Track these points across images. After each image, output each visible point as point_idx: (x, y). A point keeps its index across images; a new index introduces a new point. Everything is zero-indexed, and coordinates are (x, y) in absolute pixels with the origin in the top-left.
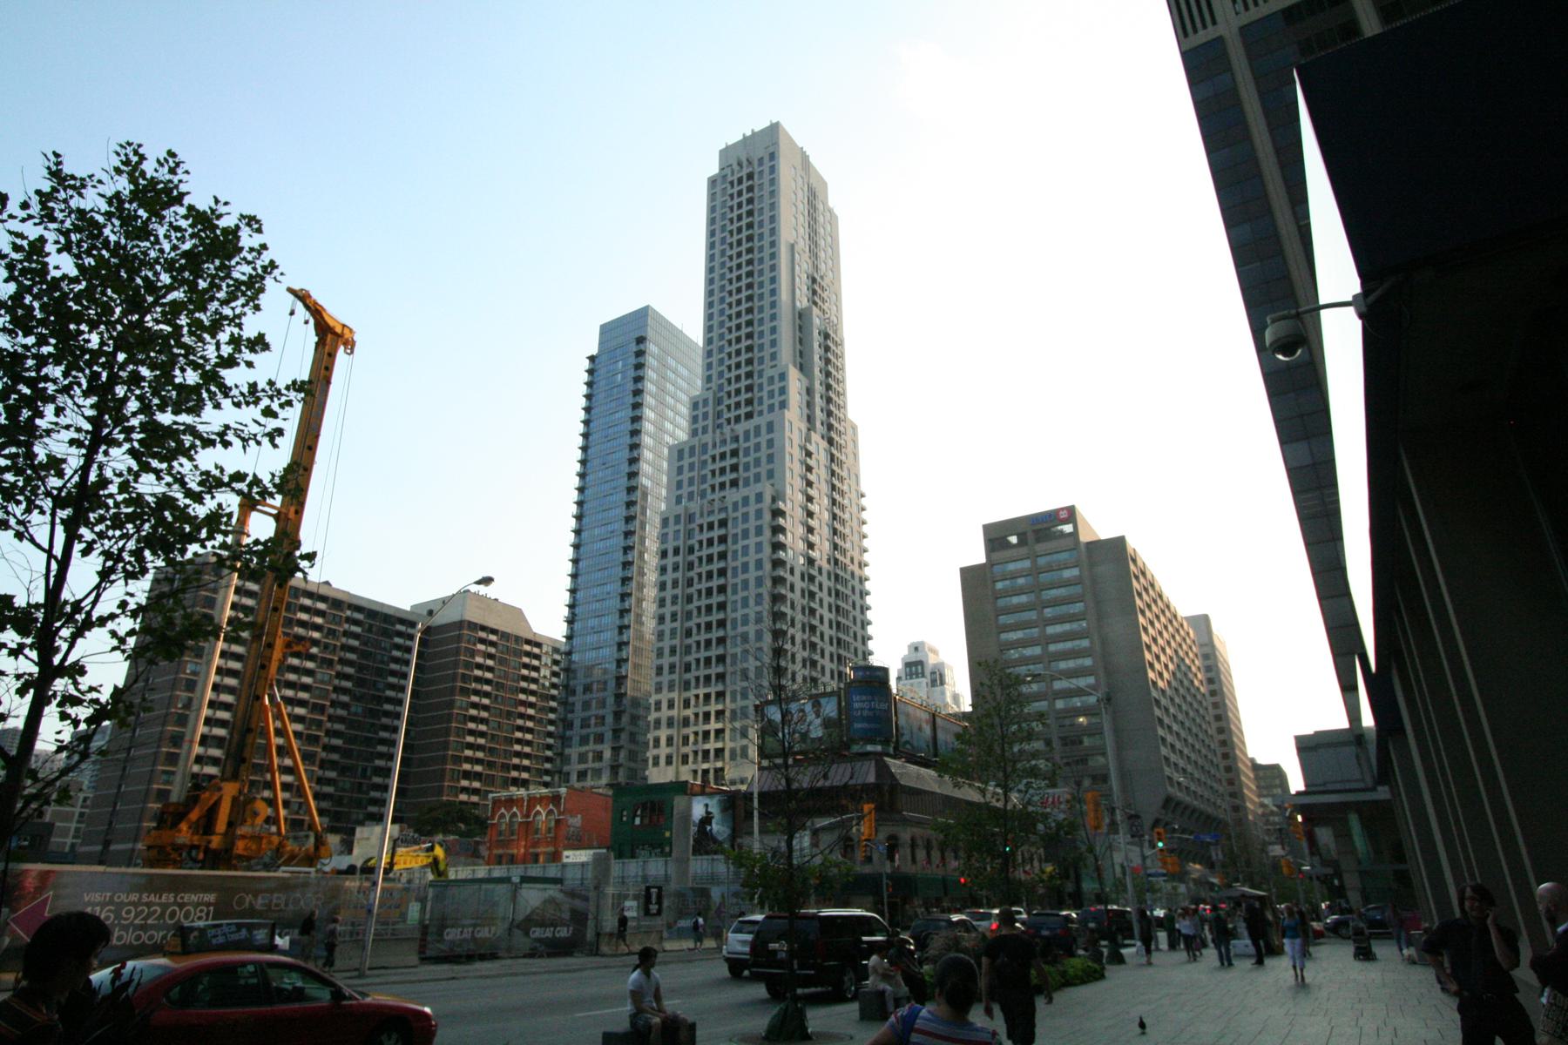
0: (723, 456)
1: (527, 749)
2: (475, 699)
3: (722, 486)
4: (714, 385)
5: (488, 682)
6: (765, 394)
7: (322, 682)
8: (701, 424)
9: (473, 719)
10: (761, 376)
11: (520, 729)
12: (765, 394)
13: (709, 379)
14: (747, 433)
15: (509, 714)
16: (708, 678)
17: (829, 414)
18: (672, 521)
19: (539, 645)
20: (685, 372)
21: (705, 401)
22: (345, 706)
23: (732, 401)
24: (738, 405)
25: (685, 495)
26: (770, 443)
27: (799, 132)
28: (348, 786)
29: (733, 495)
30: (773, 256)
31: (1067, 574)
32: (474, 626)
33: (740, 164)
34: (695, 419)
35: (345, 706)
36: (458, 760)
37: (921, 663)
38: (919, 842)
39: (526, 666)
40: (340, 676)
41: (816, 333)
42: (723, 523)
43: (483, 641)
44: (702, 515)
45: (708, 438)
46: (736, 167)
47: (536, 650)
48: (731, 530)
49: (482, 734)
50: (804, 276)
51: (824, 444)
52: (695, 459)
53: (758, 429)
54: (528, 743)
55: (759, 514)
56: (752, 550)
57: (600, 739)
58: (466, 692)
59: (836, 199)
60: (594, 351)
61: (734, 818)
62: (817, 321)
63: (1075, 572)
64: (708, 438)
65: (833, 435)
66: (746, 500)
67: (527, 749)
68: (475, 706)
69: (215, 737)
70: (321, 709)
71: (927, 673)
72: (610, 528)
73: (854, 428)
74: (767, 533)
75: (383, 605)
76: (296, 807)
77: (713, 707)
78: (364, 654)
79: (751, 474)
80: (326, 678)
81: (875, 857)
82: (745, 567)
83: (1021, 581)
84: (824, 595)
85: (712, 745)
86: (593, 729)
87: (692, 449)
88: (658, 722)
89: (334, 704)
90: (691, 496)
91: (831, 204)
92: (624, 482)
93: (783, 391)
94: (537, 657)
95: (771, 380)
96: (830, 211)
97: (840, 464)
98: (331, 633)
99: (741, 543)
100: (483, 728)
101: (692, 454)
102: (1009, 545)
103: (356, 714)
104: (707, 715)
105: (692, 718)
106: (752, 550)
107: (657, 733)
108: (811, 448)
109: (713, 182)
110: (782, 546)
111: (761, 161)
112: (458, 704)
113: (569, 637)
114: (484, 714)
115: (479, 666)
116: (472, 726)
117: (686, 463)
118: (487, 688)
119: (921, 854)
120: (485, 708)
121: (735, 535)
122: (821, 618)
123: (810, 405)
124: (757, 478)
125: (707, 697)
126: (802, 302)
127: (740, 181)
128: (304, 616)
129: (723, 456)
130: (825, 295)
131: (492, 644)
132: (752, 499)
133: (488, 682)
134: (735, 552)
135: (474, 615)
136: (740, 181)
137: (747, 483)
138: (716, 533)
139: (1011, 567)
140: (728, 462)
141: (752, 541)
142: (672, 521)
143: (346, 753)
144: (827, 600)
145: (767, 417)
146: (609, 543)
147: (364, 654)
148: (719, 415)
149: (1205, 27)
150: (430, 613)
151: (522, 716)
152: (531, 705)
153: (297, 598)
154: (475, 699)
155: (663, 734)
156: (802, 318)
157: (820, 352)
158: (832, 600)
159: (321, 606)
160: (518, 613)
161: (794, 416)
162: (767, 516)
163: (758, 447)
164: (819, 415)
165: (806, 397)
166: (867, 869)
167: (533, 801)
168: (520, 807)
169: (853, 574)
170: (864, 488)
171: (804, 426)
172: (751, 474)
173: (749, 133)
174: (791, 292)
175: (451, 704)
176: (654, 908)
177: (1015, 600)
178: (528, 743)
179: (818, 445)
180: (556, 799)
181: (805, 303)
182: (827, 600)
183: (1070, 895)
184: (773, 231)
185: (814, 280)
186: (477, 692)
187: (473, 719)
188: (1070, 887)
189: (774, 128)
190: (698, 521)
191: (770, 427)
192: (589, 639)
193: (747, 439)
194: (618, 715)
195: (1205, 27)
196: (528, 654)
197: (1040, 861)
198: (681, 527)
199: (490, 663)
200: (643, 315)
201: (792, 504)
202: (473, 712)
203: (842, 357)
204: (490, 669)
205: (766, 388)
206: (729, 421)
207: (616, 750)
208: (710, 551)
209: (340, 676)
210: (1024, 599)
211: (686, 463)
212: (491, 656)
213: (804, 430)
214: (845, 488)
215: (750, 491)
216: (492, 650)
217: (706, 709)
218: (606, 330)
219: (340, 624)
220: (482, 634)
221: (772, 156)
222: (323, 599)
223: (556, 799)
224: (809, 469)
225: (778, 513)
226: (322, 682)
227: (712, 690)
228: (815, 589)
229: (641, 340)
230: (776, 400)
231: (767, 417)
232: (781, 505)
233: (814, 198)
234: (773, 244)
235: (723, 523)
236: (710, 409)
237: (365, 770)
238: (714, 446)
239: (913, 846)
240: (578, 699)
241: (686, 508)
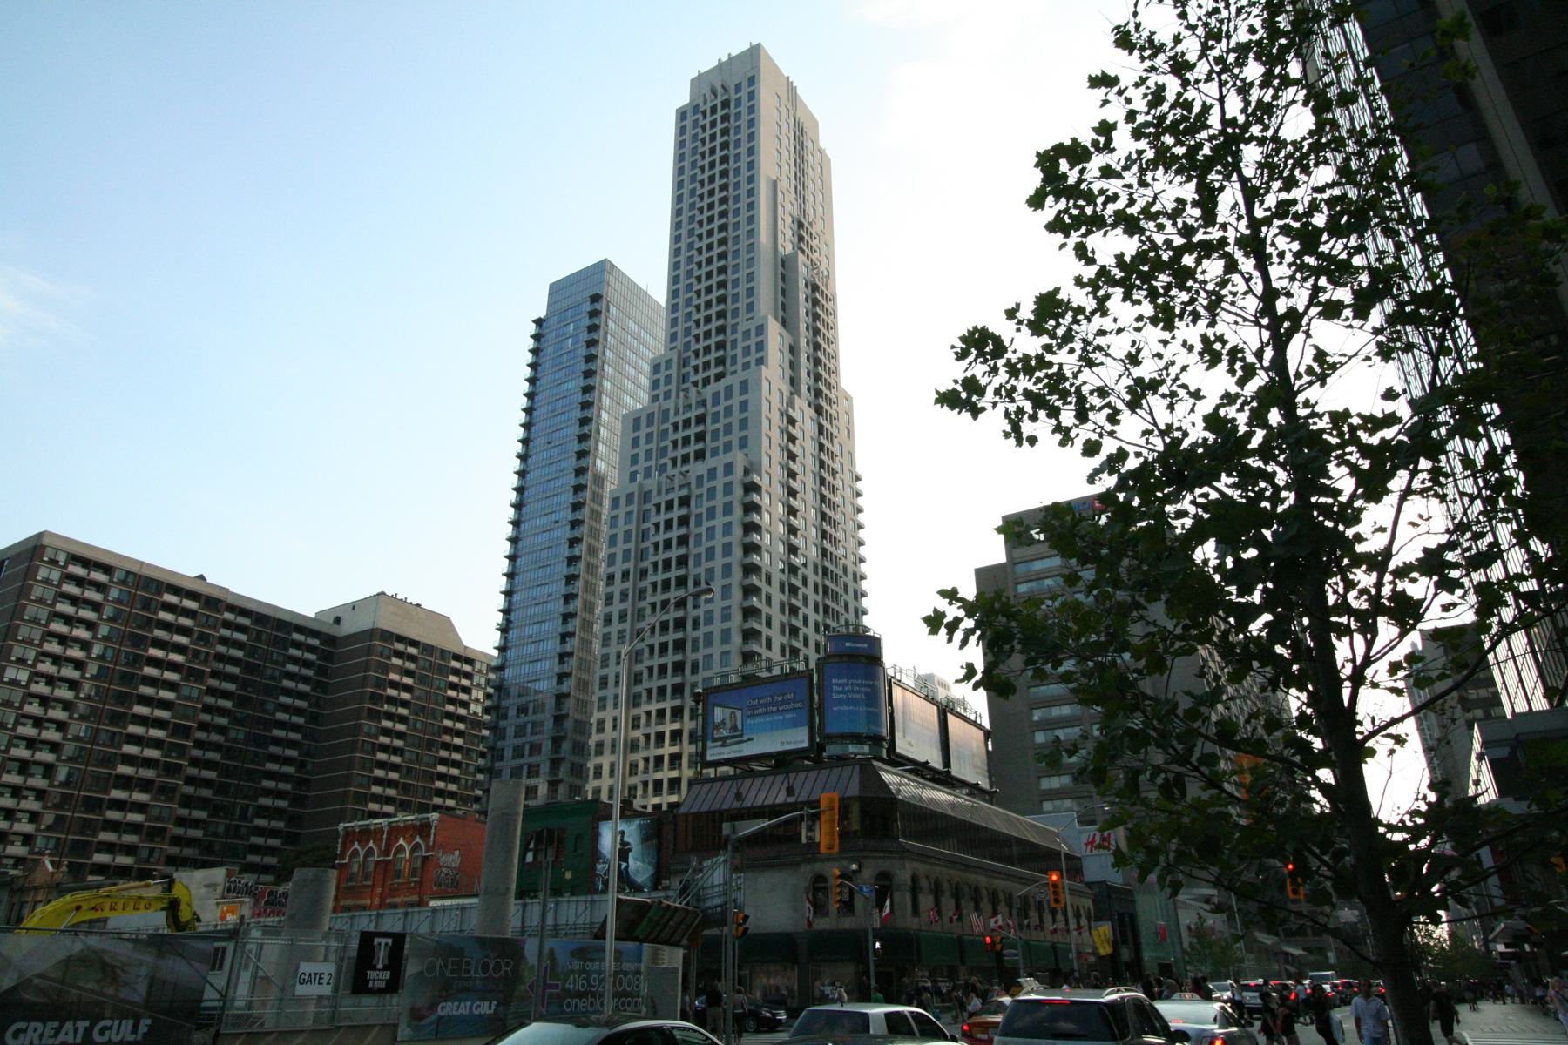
0: (687, 423)
1: (452, 787)
2: (387, 724)
3: (685, 459)
4: (679, 344)
5: (404, 704)
6: (739, 351)
7: (189, 698)
8: (663, 388)
9: (385, 748)
10: (734, 331)
11: (444, 762)
12: (739, 351)
13: (673, 337)
14: (716, 395)
15: (430, 744)
16: (662, 691)
17: (818, 378)
18: (623, 501)
19: (470, 661)
20: (649, 340)
21: (668, 363)
22: (222, 730)
23: (700, 362)
24: (707, 366)
25: (641, 471)
26: (744, 406)
27: (785, 58)
28: (221, 829)
29: (698, 468)
30: (751, 193)
32: (387, 636)
33: (714, 92)
34: (655, 384)
35: (222, 730)
36: (364, 798)
38: (924, 883)
39: (453, 686)
40: (212, 691)
41: (802, 283)
42: (684, 501)
43: (399, 654)
44: (659, 493)
45: (670, 405)
46: (709, 96)
47: (467, 668)
48: (694, 509)
49: (395, 767)
50: (789, 220)
51: (810, 412)
52: (654, 429)
53: (729, 389)
54: (454, 779)
55: (728, 488)
56: (719, 531)
57: (533, 771)
58: (375, 715)
59: (828, 139)
60: (542, 314)
61: (659, 849)
62: (802, 270)
64: (670, 405)
65: (822, 402)
66: (712, 473)
67: (452, 787)
68: (387, 732)
69: (199, 798)
70: (184, 731)
72: (555, 517)
73: (848, 399)
74: (738, 512)
75: (276, 608)
76: (145, 854)
77: (669, 727)
78: (249, 668)
79: (720, 444)
80: (195, 694)
81: (859, 903)
82: (710, 553)
84: (810, 591)
85: (666, 774)
86: (527, 760)
87: (650, 416)
88: (600, 746)
89: (203, 726)
90: (648, 473)
91: (823, 144)
92: (572, 462)
93: (761, 346)
94: (468, 676)
95: (747, 334)
96: (821, 152)
97: (831, 438)
98: (203, 638)
99: (706, 524)
100: (396, 759)
101: (650, 422)
102: (1032, 542)
103: (235, 741)
104: (660, 737)
105: (642, 739)
106: (719, 531)
107: (599, 760)
108: (796, 415)
109: (682, 114)
110: (756, 528)
111: (738, 88)
112: (366, 729)
113: (502, 649)
114: (399, 743)
115: (394, 685)
116: (382, 756)
117: (643, 433)
118: (403, 711)
119: (926, 901)
120: (400, 735)
121: (699, 516)
122: (806, 618)
123: (793, 366)
124: (728, 447)
125: (661, 713)
126: (786, 248)
127: (714, 110)
128: (167, 616)
129: (687, 423)
130: (814, 243)
131: (412, 658)
132: (720, 471)
133: (404, 704)
134: (699, 536)
136: (714, 110)
137: (715, 452)
138: (676, 513)
139: (1037, 566)
140: (693, 430)
141: (719, 521)
142: (623, 501)
143: (221, 789)
144: (812, 597)
145: (741, 375)
146: (554, 534)
147: (249, 668)
148: (684, 378)
150: (338, 620)
151: (446, 746)
152: (459, 734)
153: (160, 594)
154: (387, 724)
155: (605, 761)
156: (785, 267)
157: (807, 307)
158: (819, 598)
159: (191, 604)
160: (444, 623)
161: (773, 374)
162: (738, 491)
163: (728, 411)
164: (805, 380)
165: (788, 356)
166: (847, 923)
167: (395, 832)
168: (378, 841)
169: (845, 569)
170: (860, 469)
171: (786, 388)
172: (720, 444)
173: (725, 58)
174: (771, 233)
175: (357, 729)
176: (378, 977)
178: (454, 779)
179: (803, 411)
180: (423, 829)
181: (789, 249)
182: (812, 597)
183: (1127, 964)
184: (751, 165)
185: (801, 225)
186: (390, 716)
187: (385, 748)
188: (1126, 954)
189: (755, 52)
190: (655, 500)
191: (744, 387)
192: (526, 650)
193: (716, 402)
194: (557, 741)
196: (456, 672)
197: (1089, 918)
198: (634, 508)
199: (408, 681)
200: (602, 269)
201: (771, 479)
202: (384, 740)
203: (834, 314)
204: (407, 688)
205: (740, 345)
206: (695, 384)
207: (553, 785)
208: (668, 535)
209: (212, 691)
211: (643, 433)
212: (409, 673)
213: (786, 394)
214: (837, 466)
215: (717, 462)
216: (411, 666)
217: (660, 729)
218: (557, 289)
219: (214, 628)
220: (400, 646)
221: (752, 81)
222: (193, 595)
223: (423, 829)
224: (792, 456)
225: (751, 488)
227: (668, 704)
228: (798, 603)
229: (596, 298)
230: (752, 358)
231: (741, 375)
232: (756, 478)
233: (801, 134)
234: (751, 179)
235: (684, 501)
236: (674, 371)
237: (245, 809)
238: (677, 412)
239: (915, 889)
240: (510, 725)
241: (641, 486)
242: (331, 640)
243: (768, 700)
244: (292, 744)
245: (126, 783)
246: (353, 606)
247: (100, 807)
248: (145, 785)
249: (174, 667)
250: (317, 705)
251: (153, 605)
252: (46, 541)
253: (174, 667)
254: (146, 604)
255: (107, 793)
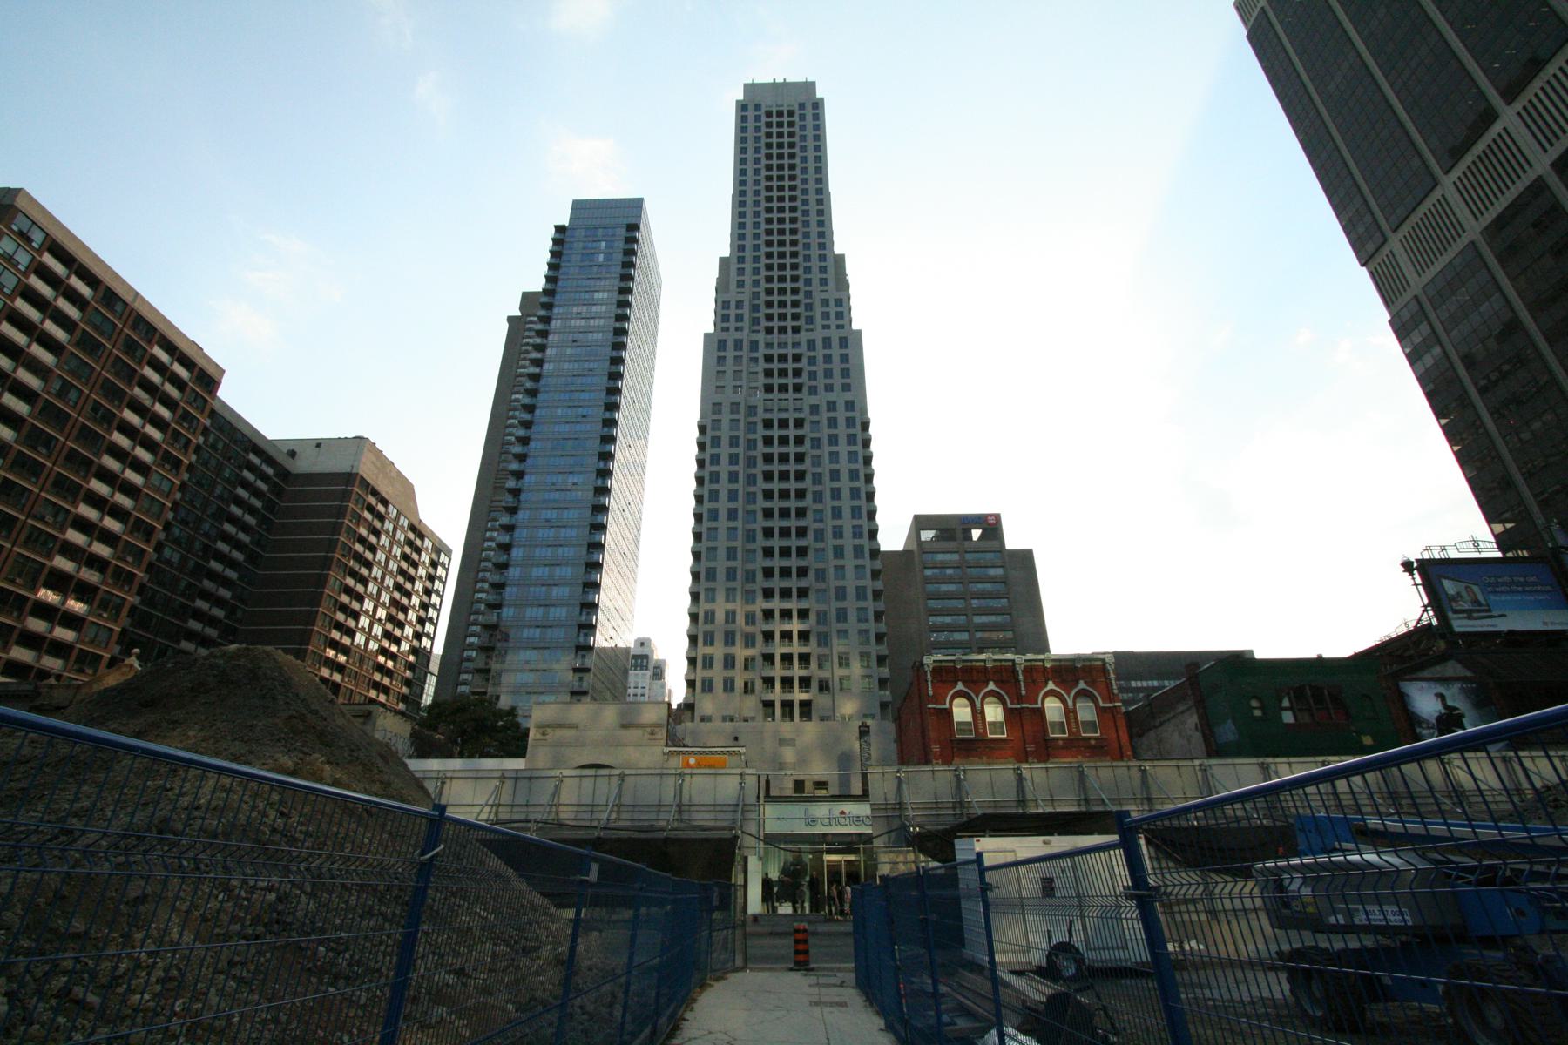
31: (992, 572)
32: (365, 485)
37: (646, 657)
63: (999, 571)
71: (651, 667)
83: (949, 571)
98: (186, 416)
103: (168, 562)
135: (367, 470)
139: (940, 557)
149: (1536, 95)
177: (944, 588)
195: (1536, 95)
210: (952, 587)
226: (158, 490)
242: (284, 474)
243: (1507, 579)
244: (226, 582)
245: (59, 581)
246: (318, 444)
247: (21, 609)
248: (84, 591)
249: (148, 444)
250: (258, 544)
251: (139, 353)
252: (20, 203)
253: (148, 444)
254: (130, 347)
255: (35, 590)
